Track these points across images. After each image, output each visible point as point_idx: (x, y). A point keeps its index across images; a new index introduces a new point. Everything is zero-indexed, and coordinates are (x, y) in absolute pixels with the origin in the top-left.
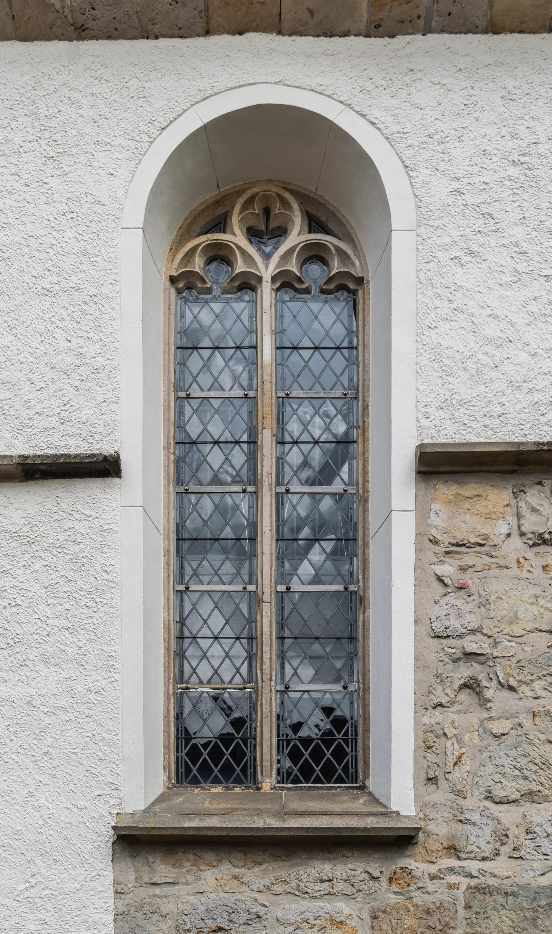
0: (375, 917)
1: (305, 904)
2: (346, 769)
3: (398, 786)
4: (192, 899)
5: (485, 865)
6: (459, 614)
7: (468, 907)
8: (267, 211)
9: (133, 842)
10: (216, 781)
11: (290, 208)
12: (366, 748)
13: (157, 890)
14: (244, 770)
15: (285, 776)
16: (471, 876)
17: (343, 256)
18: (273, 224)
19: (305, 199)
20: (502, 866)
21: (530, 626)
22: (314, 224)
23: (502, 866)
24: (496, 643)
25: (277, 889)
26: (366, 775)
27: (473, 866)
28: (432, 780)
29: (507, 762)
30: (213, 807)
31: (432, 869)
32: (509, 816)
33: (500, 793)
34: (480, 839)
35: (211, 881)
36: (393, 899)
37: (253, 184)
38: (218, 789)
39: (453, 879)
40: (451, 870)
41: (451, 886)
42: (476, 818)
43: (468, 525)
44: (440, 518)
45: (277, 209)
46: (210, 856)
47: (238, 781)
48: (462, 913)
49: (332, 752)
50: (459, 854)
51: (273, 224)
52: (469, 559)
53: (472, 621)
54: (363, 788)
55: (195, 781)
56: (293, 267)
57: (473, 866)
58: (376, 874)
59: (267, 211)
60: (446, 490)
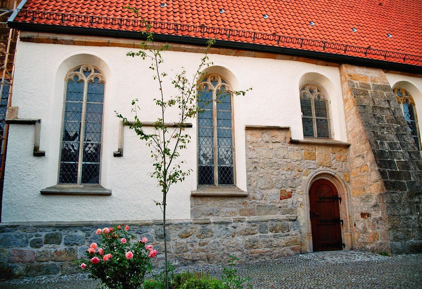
0: (240, 211)
1: (227, 209)
2: (231, 182)
3: (241, 183)
4: (206, 208)
5: (260, 201)
6: (253, 154)
7: (257, 209)
8: (214, 78)
9: (194, 196)
10: (206, 184)
11: (218, 78)
12: (236, 178)
13: (199, 206)
14: (212, 181)
15: (220, 183)
16: (257, 203)
17: (228, 87)
18: (215, 80)
19: (221, 76)
20: (263, 201)
21: (266, 157)
22: (223, 81)
23: (263, 201)
24: (259, 160)
25: (222, 206)
26: (236, 183)
27: (258, 201)
28: (250, 185)
29: (263, 182)
30: (208, 190)
31: (250, 202)
32: (264, 192)
33: (262, 188)
34: (258, 196)
35: (209, 204)
36: (244, 208)
37: (212, 74)
38: (207, 186)
39: (254, 204)
40: (254, 202)
41: (254, 205)
42: (258, 192)
43: (254, 139)
44: (249, 138)
45: (216, 78)
46: (227, 199)
47: (211, 184)
48: (256, 211)
49: (227, 176)
50: (166, 155)
51: (215, 80)
52: (255, 145)
53: (255, 156)
54: (235, 186)
55: (202, 184)
56: (219, 88)
57: (258, 201)
58: (240, 203)
59: (214, 78)
60: (250, 132)
